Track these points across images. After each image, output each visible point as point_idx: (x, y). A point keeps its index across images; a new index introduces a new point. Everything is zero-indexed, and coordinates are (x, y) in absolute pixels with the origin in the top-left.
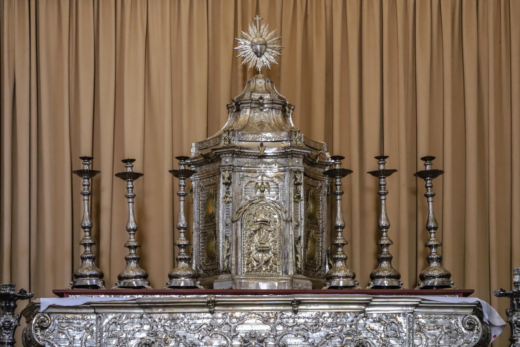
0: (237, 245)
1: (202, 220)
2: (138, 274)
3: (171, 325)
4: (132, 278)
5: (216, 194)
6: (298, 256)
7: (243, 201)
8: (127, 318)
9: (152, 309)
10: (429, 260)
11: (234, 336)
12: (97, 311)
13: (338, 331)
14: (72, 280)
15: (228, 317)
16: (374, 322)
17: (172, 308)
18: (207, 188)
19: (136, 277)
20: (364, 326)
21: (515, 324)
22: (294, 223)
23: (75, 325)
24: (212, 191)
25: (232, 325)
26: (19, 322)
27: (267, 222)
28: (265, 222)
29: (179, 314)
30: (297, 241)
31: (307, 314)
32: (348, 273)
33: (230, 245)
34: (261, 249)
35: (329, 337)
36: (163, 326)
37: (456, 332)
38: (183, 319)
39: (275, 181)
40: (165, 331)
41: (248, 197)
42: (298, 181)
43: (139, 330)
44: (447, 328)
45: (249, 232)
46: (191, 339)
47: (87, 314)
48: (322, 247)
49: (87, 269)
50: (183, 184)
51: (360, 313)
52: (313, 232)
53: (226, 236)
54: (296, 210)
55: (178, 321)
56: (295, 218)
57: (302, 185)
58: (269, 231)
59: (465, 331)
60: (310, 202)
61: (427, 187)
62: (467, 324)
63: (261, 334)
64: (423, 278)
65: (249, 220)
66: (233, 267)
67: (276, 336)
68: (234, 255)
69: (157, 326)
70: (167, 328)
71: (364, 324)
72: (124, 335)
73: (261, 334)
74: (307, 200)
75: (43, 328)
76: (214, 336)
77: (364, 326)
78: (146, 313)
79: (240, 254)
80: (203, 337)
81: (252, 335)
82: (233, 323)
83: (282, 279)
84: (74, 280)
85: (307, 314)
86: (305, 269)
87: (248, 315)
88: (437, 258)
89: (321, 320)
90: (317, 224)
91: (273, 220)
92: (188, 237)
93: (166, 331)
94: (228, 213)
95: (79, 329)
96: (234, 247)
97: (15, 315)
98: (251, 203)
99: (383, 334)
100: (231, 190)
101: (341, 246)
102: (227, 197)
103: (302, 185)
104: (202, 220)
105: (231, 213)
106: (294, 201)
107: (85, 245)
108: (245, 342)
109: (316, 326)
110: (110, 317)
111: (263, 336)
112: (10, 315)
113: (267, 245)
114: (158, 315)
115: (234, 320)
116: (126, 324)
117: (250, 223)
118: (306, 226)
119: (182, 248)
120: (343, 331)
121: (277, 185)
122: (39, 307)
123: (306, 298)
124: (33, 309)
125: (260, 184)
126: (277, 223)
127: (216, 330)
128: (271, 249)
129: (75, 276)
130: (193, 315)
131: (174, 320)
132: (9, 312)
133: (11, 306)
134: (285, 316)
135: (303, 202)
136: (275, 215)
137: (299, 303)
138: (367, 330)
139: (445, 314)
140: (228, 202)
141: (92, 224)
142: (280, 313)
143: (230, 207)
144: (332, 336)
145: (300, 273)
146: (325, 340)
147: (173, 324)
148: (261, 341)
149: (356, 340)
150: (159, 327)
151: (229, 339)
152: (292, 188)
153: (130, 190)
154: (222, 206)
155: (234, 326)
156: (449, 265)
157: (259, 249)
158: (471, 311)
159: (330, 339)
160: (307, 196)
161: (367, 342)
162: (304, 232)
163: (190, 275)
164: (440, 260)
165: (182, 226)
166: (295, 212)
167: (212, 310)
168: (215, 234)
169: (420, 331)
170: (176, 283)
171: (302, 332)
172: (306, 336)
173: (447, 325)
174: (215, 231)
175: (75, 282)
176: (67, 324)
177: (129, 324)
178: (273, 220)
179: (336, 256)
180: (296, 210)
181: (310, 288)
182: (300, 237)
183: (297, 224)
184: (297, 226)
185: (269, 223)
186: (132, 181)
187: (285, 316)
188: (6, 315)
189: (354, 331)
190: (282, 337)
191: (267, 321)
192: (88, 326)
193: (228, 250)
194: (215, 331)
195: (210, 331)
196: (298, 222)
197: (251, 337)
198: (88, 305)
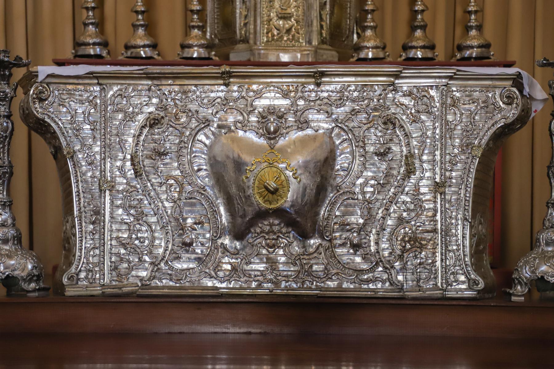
2: (147, 42)
3: (182, 98)
4: (140, 47)
6: (323, 24)
8: (134, 90)
10: (468, 29)
12: (101, 81)
14: (74, 48)
16: (404, 95)
19: (144, 46)
26: (15, 93)
29: (191, 85)
31: (332, 87)
32: (378, 43)
35: (354, 113)
36: (173, 99)
38: (195, 92)
40: (176, 104)
44: (483, 102)
49: (90, 36)
51: (389, 86)
55: (190, 94)
59: (502, 106)
64: (460, 48)
66: (252, 36)
69: (167, 100)
75: (41, 100)
80: (217, 112)
81: (271, 110)
83: (305, 50)
84: (77, 48)
85: (332, 87)
86: (331, 38)
88: (477, 26)
95: (81, 102)
97: (11, 85)
107: (87, 9)
109: (341, 101)
110: (115, 88)
113: (289, 11)
116: (132, 97)
124: (31, 77)
129: (77, 44)
130: (206, 88)
131: (185, 93)
134: (307, 89)
137: (323, 74)
139: (482, 86)
145: (326, 43)
148: (281, 117)
150: (169, 100)
156: (489, 34)
163: (203, 44)
164: (479, 28)
169: (453, 106)
170: (188, 53)
173: (484, 99)
175: (76, 51)
176: (68, 96)
179: (366, 24)
181: (336, 60)
187: (307, 89)
192: (91, 98)
193: (246, 17)
198: (91, 75)
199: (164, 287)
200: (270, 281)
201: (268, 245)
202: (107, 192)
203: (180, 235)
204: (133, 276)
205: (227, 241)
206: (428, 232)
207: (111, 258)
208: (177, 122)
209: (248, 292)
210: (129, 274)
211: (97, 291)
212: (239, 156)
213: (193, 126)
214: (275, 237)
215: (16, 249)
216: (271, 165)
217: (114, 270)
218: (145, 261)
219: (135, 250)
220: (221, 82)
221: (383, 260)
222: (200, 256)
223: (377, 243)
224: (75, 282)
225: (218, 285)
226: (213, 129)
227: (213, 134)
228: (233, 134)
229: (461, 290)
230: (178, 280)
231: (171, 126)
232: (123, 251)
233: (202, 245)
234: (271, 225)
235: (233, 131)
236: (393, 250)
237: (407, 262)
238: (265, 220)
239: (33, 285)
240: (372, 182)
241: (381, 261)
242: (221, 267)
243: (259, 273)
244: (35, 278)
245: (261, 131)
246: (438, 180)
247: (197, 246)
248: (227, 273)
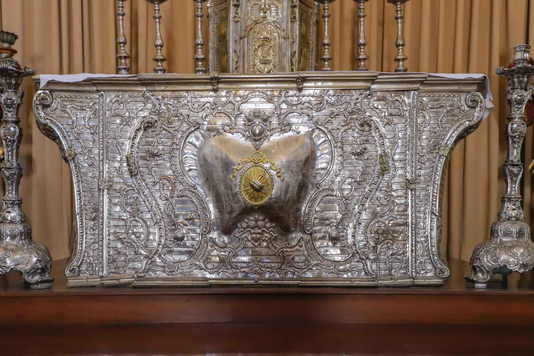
0: (244, 58)
1: (216, 40)
5: (227, 17)
6: (294, 67)
7: (249, 21)
9: (154, 87)
11: (237, 114)
13: (342, 110)
15: (232, 95)
17: (174, 86)
18: (220, 12)
20: (369, 104)
21: (515, 101)
22: (291, 40)
23: (78, 104)
24: (224, 15)
25: (236, 103)
27: (268, 39)
28: (266, 39)
30: (293, 55)
33: (238, 58)
34: (264, 61)
37: (458, 110)
39: (275, 4)
40: (168, 109)
41: (253, 17)
42: (294, 3)
43: (143, 109)
45: (254, 47)
46: (194, 118)
47: (90, 92)
48: (311, 63)
50: (200, 7)
52: (305, 50)
53: (235, 51)
54: (292, 28)
55: (181, 100)
56: (291, 35)
57: (298, 7)
58: (271, 47)
60: (303, 24)
61: (397, 11)
62: (471, 101)
63: (265, 113)
65: (254, 37)
67: (280, 115)
68: (241, 67)
69: (160, 104)
70: (170, 106)
71: (368, 103)
72: (127, 114)
73: (265, 113)
74: (301, 22)
75: (45, 107)
76: (217, 115)
77: (369, 104)
78: (149, 90)
79: (246, 66)
80: (206, 116)
81: (257, 114)
82: (237, 102)
87: (252, 93)
89: (326, 98)
90: (308, 43)
91: (273, 37)
92: (206, 53)
93: (169, 110)
94: (237, 31)
96: (242, 58)
98: (256, 23)
99: (386, 112)
100: (239, 11)
101: (327, 61)
102: (236, 17)
103: (298, 7)
104: (216, 40)
105: (239, 31)
106: (291, 21)
108: (249, 121)
111: (267, 115)
112: (12, 92)
113: (268, 58)
114: (161, 93)
115: (238, 99)
117: (255, 40)
118: (300, 43)
119: (200, 61)
120: (348, 109)
121: (277, 7)
122: (39, 83)
123: (311, 75)
125: (263, 6)
126: (277, 40)
127: (220, 108)
128: (271, 62)
132: (11, 89)
133: (12, 83)
135: (298, 23)
136: (275, 33)
138: (371, 108)
140: (237, 21)
141: (126, 40)
142: (285, 90)
143: (239, 26)
144: (337, 115)
146: (330, 119)
147: (176, 102)
148: (265, 120)
149: (360, 118)
151: (233, 119)
152: (290, 9)
153: (157, 11)
154: (232, 25)
155: (238, 105)
157: (262, 62)
158: (475, 88)
159: (334, 118)
160: (301, 18)
161: (372, 120)
162: (299, 48)
165: (199, 42)
166: (291, 30)
167: (215, 88)
168: (227, 50)
171: (307, 111)
172: (310, 114)
174: (226, 48)
177: (133, 103)
178: (273, 37)
180: (292, 28)
182: (295, 51)
183: (293, 40)
184: (293, 42)
185: (271, 40)
186: (158, 4)
188: (8, 92)
189: (359, 109)
190: (286, 116)
191: (271, 99)
194: (218, 110)
195: (213, 109)
196: (293, 39)
197: (255, 116)
199: (157, 279)
200: (256, 272)
201: (253, 239)
202: (106, 191)
203: (172, 231)
204: (129, 268)
205: (214, 235)
206: (399, 225)
207: (109, 252)
208: (169, 126)
209: (235, 282)
210: (125, 266)
211: (96, 281)
212: (227, 156)
213: (184, 129)
214: (260, 231)
215: (23, 244)
216: (256, 164)
217: (112, 263)
218: (141, 254)
219: (131, 245)
220: (210, 87)
221: (359, 252)
222: (191, 249)
223: (353, 236)
224: (76, 274)
225: (208, 276)
226: (202, 131)
227: (203, 136)
228: (221, 136)
229: (428, 278)
230: (170, 272)
231: (164, 129)
232: (119, 245)
233: (193, 239)
234: (256, 221)
235: (222, 134)
236: (367, 242)
237: (380, 253)
238: (251, 216)
239: (37, 278)
240: (349, 180)
241: (357, 253)
242: (211, 259)
243: (245, 265)
244: (39, 271)
245: (247, 133)
246: (409, 176)
247: (188, 240)
248: (216, 265)
